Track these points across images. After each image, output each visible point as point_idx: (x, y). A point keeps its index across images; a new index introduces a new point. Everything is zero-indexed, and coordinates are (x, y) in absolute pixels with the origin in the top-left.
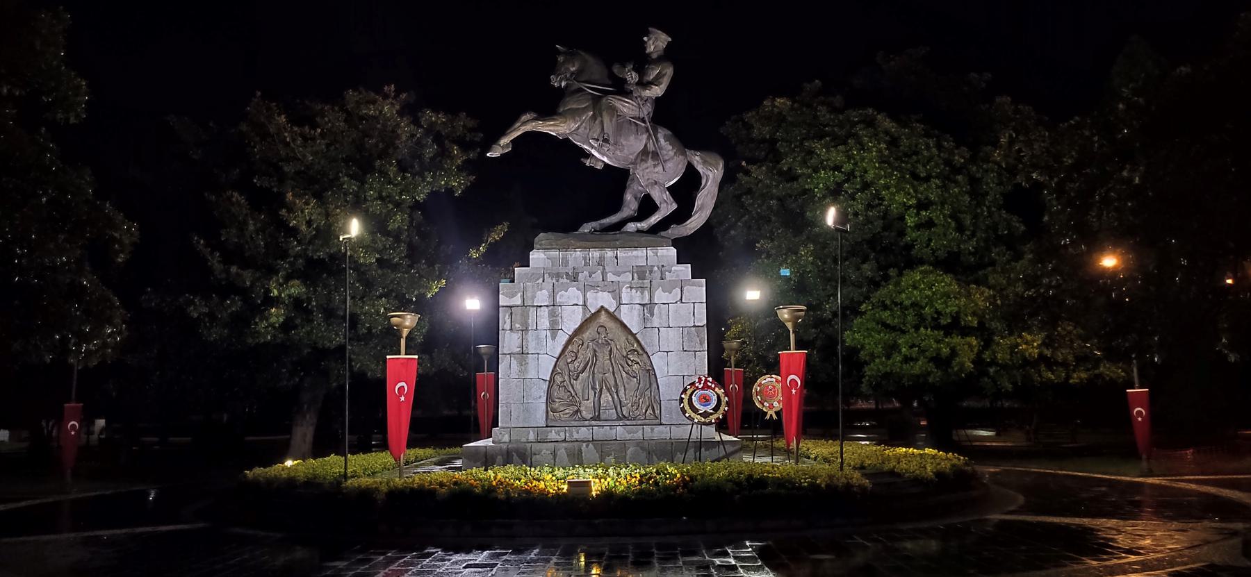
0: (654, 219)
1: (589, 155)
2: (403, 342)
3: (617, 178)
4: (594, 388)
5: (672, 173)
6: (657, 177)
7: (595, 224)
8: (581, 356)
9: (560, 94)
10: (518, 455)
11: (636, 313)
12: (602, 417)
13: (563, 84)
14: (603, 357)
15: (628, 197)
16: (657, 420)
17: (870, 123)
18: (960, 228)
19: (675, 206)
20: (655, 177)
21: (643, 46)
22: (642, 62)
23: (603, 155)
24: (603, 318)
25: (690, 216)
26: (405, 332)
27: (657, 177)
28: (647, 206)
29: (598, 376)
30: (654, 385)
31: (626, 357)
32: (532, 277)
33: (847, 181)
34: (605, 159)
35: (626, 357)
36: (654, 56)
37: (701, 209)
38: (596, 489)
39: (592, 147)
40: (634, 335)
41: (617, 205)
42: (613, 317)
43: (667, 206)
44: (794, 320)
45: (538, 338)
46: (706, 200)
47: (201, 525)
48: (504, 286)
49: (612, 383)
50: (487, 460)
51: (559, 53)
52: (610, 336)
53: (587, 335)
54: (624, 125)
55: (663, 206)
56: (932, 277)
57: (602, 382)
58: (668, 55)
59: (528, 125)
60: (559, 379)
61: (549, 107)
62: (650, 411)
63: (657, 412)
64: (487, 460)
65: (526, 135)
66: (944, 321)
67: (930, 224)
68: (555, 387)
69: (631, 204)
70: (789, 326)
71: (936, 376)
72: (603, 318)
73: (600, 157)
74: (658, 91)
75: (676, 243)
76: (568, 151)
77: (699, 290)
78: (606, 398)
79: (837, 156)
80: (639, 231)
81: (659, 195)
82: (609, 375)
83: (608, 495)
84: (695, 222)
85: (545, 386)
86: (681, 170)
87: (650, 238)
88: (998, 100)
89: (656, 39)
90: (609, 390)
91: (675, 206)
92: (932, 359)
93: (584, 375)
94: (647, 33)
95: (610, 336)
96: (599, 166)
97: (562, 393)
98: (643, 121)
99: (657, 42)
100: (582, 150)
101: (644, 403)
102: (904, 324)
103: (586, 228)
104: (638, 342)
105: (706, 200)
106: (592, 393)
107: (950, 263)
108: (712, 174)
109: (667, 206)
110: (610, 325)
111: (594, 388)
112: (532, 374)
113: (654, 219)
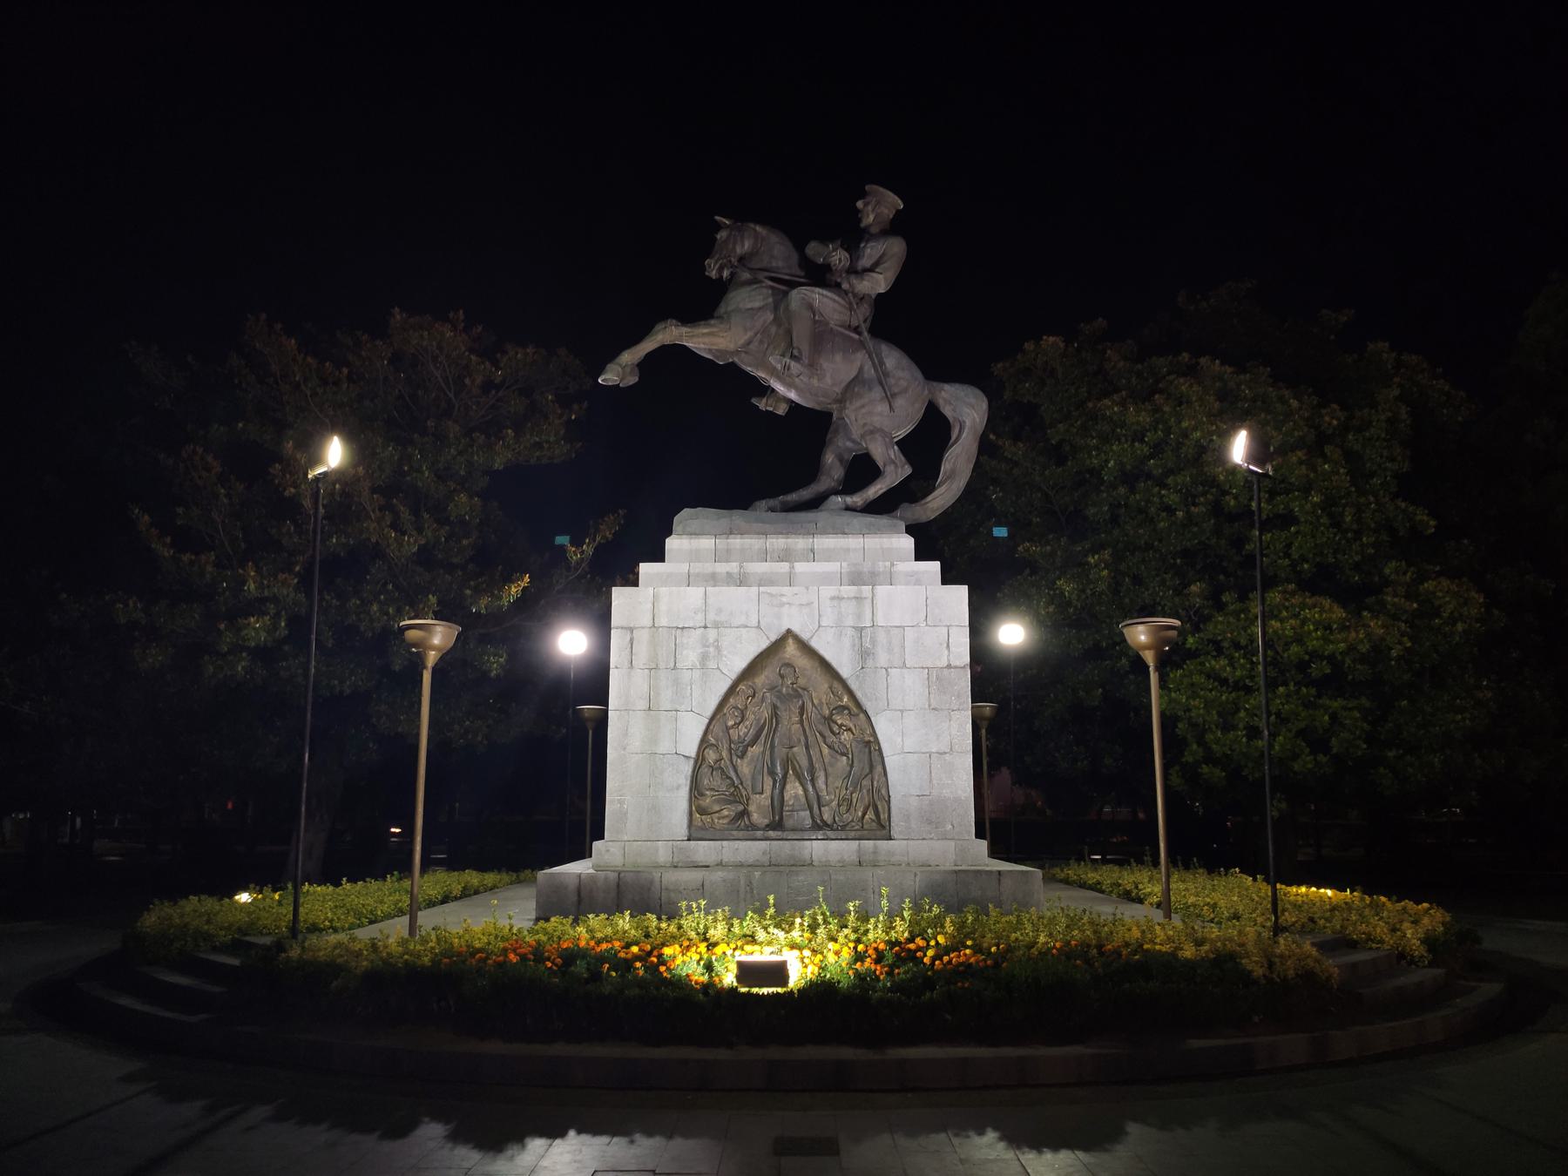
0: (875, 490)
1: (766, 391)
2: (427, 677)
3: (812, 426)
4: (772, 773)
5: (902, 418)
6: (879, 420)
8: (750, 717)
9: (720, 289)
10: (634, 894)
11: (847, 642)
12: (788, 823)
13: (726, 274)
14: (790, 721)
15: (829, 458)
16: (882, 829)
17: (1191, 371)
18: (1336, 524)
19: (908, 470)
20: (877, 421)
21: (856, 215)
22: (853, 237)
23: (790, 386)
24: (791, 649)
25: (933, 489)
26: (432, 657)
27: (879, 420)
28: (862, 470)
29: (781, 752)
30: (879, 769)
31: (829, 720)
32: (668, 580)
33: (1151, 456)
34: (792, 395)
35: (829, 720)
36: (874, 230)
37: (951, 475)
38: (799, 974)
39: (773, 372)
41: (812, 471)
42: (806, 648)
43: (895, 472)
44: (1157, 646)
45: (676, 682)
46: (958, 462)
48: (620, 595)
49: (804, 762)
50: (582, 902)
51: (719, 227)
52: (801, 681)
53: (761, 680)
54: (822, 337)
55: (890, 469)
56: (1296, 600)
58: (895, 227)
59: (668, 334)
60: (711, 756)
61: (703, 304)
62: (870, 815)
63: (883, 816)
64: (582, 902)
65: (663, 349)
66: (1318, 669)
67: (1287, 520)
68: (705, 770)
69: (833, 467)
70: (1149, 657)
71: (1305, 762)
73: (787, 390)
74: (879, 283)
76: (735, 384)
78: (794, 790)
79: (1139, 416)
81: (880, 451)
82: (800, 752)
83: (820, 992)
84: (942, 498)
85: (688, 768)
86: (918, 412)
87: (870, 519)
88: (1371, 346)
89: (878, 203)
90: (799, 777)
91: (908, 470)
92: (1301, 733)
93: (755, 750)
94: (863, 195)
95: (801, 681)
96: (782, 410)
97: (717, 781)
98: (856, 330)
99: (879, 206)
100: (755, 380)
101: (860, 799)
102: (1252, 678)
105: (958, 462)
106: (768, 782)
107: (1321, 581)
108: (967, 410)
109: (895, 472)
110: (802, 662)
111: (772, 773)
112: (665, 746)
113: (875, 490)
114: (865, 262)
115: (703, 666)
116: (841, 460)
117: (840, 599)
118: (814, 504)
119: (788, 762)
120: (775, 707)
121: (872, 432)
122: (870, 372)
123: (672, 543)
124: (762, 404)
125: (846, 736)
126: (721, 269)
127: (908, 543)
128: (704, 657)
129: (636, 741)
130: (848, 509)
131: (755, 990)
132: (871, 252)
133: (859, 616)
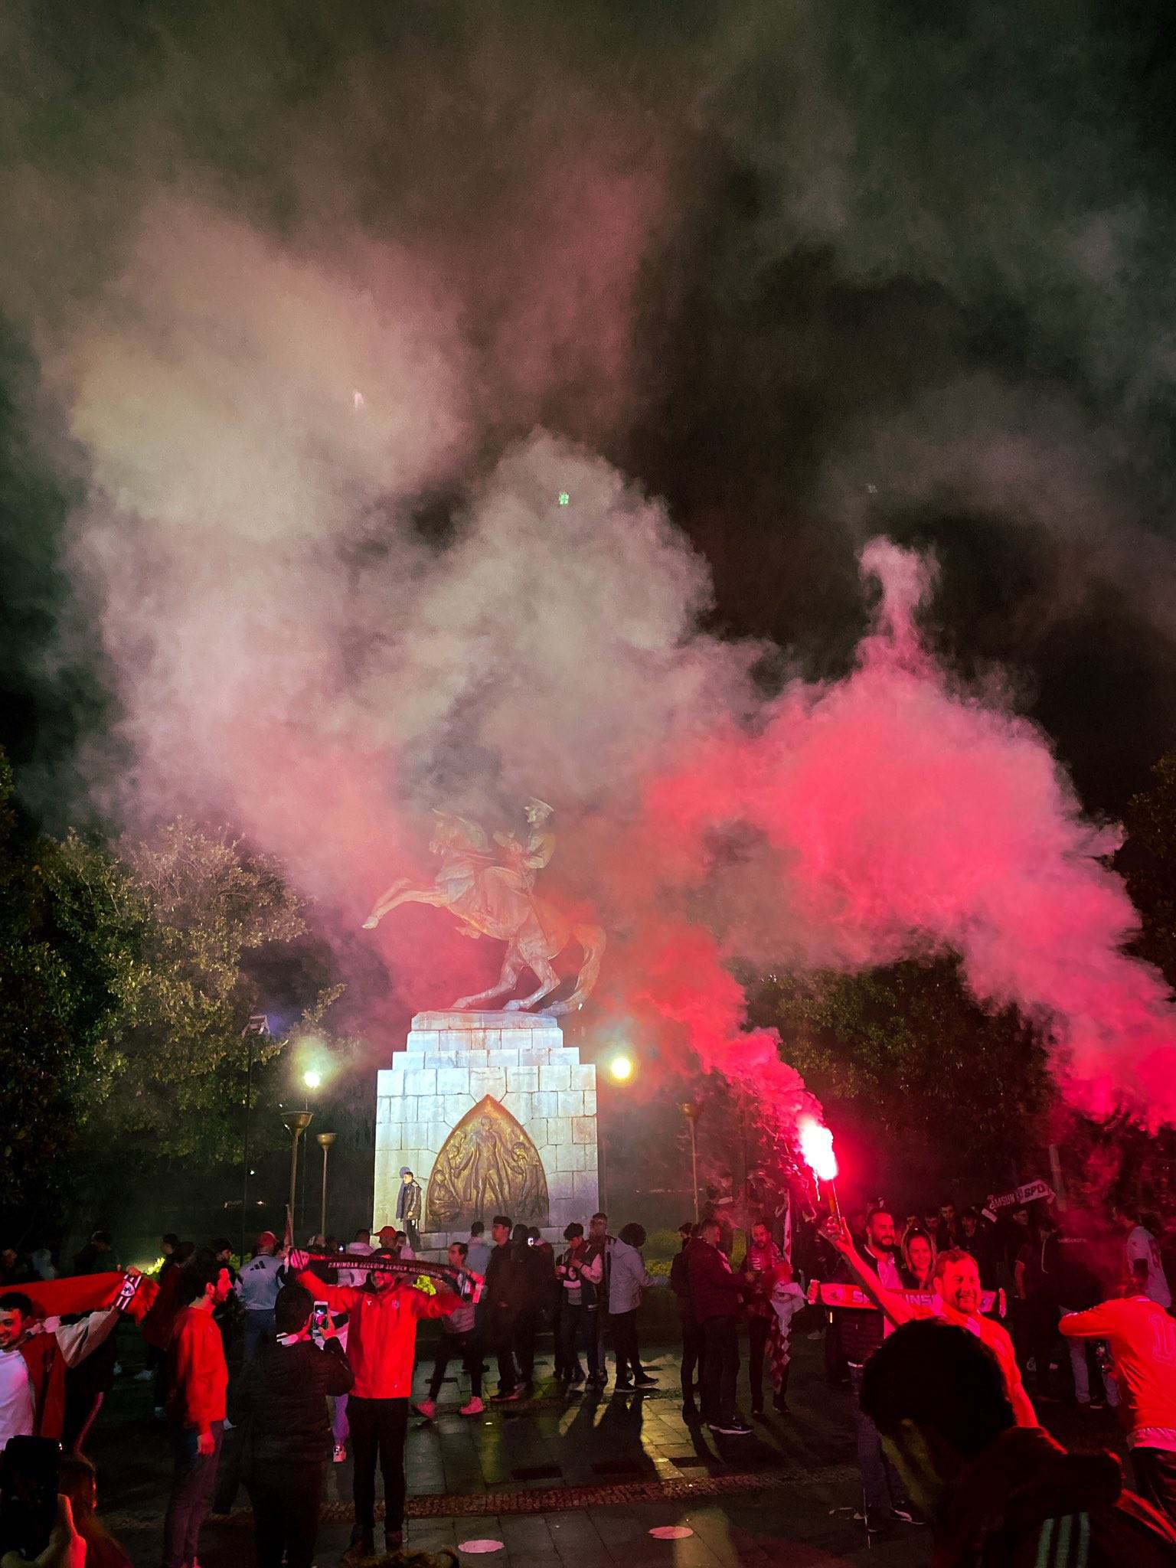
0: (537, 996)
1: (463, 924)
7: (470, 999)
11: (523, 1103)
15: (507, 969)
24: (489, 1108)
28: (528, 983)
29: (482, 1172)
31: (511, 1153)
39: (473, 917)
40: (521, 1128)
41: (496, 977)
42: (498, 1107)
46: (588, 974)
47: (1061, 1449)
49: (496, 1180)
53: (469, 1128)
55: (546, 983)
57: (486, 1180)
72: (489, 1108)
75: (562, 1021)
77: (386, 1082)
80: (521, 1009)
81: (540, 969)
90: (493, 1189)
93: (466, 1172)
103: (462, 1003)
104: (525, 1134)
111: (476, 1187)
113: (537, 996)
114: (532, 848)
115: (435, 1120)
116: (514, 970)
117: (519, 1074)
118: (497, 1004)
119: (486, 1180)
120: (478, 1145)
121: (536, 959)
122: (534, 920)
123: (411, 1037)
124: (463, 931)
125: (521, 1162)
126: (440, 848)
127: (558, 1034)
128: (436, 1114)
129: (394, 1170)
130: (521, 1009)
131: (98, 1406)
132: (535, 842)
133: (530, 1085)
